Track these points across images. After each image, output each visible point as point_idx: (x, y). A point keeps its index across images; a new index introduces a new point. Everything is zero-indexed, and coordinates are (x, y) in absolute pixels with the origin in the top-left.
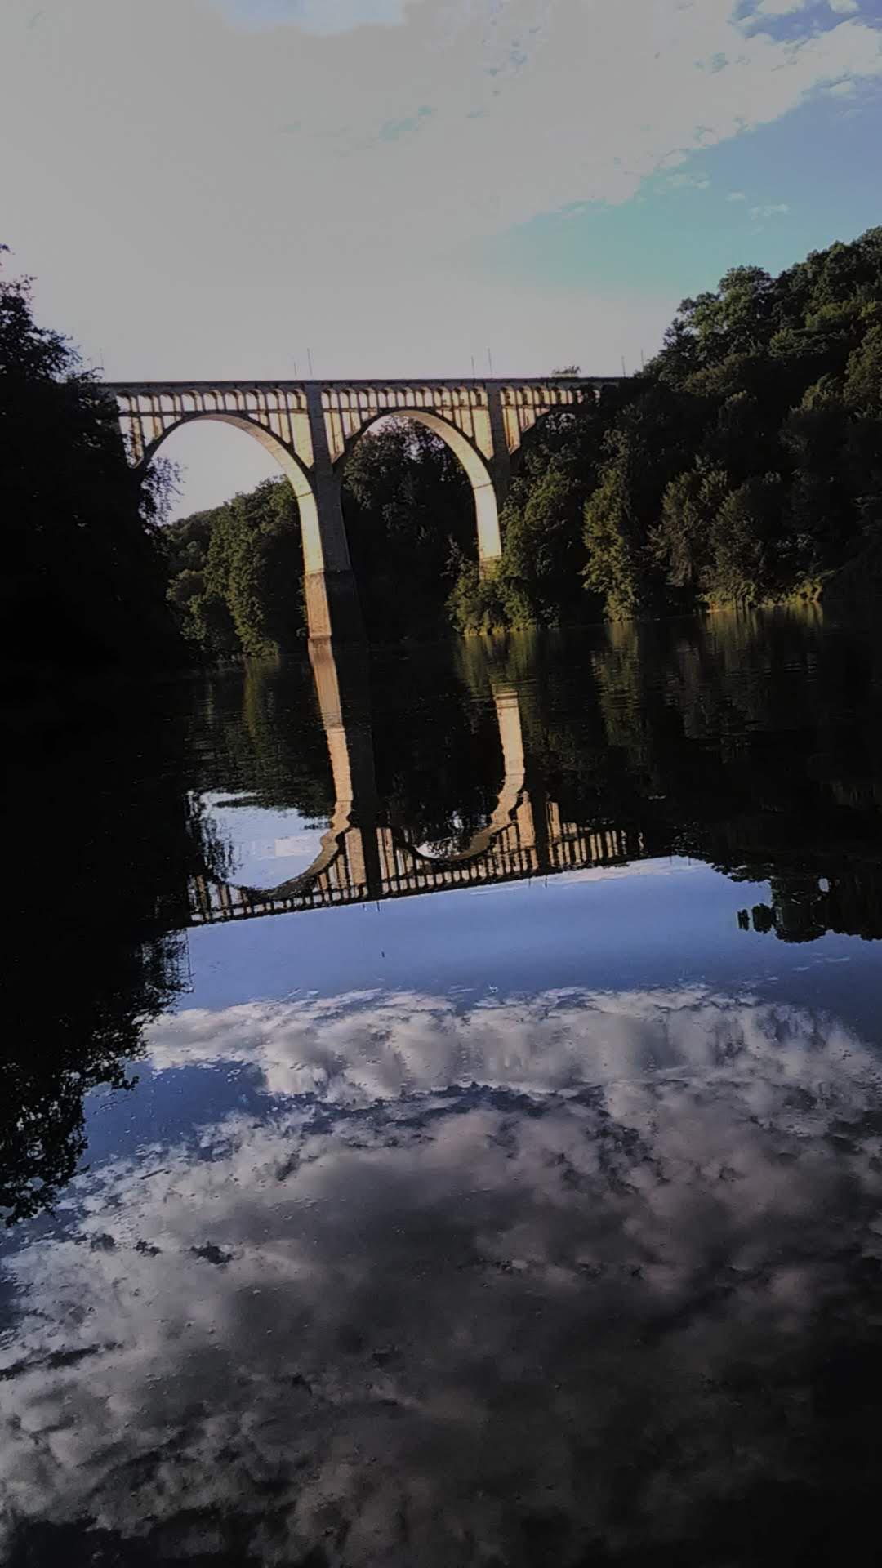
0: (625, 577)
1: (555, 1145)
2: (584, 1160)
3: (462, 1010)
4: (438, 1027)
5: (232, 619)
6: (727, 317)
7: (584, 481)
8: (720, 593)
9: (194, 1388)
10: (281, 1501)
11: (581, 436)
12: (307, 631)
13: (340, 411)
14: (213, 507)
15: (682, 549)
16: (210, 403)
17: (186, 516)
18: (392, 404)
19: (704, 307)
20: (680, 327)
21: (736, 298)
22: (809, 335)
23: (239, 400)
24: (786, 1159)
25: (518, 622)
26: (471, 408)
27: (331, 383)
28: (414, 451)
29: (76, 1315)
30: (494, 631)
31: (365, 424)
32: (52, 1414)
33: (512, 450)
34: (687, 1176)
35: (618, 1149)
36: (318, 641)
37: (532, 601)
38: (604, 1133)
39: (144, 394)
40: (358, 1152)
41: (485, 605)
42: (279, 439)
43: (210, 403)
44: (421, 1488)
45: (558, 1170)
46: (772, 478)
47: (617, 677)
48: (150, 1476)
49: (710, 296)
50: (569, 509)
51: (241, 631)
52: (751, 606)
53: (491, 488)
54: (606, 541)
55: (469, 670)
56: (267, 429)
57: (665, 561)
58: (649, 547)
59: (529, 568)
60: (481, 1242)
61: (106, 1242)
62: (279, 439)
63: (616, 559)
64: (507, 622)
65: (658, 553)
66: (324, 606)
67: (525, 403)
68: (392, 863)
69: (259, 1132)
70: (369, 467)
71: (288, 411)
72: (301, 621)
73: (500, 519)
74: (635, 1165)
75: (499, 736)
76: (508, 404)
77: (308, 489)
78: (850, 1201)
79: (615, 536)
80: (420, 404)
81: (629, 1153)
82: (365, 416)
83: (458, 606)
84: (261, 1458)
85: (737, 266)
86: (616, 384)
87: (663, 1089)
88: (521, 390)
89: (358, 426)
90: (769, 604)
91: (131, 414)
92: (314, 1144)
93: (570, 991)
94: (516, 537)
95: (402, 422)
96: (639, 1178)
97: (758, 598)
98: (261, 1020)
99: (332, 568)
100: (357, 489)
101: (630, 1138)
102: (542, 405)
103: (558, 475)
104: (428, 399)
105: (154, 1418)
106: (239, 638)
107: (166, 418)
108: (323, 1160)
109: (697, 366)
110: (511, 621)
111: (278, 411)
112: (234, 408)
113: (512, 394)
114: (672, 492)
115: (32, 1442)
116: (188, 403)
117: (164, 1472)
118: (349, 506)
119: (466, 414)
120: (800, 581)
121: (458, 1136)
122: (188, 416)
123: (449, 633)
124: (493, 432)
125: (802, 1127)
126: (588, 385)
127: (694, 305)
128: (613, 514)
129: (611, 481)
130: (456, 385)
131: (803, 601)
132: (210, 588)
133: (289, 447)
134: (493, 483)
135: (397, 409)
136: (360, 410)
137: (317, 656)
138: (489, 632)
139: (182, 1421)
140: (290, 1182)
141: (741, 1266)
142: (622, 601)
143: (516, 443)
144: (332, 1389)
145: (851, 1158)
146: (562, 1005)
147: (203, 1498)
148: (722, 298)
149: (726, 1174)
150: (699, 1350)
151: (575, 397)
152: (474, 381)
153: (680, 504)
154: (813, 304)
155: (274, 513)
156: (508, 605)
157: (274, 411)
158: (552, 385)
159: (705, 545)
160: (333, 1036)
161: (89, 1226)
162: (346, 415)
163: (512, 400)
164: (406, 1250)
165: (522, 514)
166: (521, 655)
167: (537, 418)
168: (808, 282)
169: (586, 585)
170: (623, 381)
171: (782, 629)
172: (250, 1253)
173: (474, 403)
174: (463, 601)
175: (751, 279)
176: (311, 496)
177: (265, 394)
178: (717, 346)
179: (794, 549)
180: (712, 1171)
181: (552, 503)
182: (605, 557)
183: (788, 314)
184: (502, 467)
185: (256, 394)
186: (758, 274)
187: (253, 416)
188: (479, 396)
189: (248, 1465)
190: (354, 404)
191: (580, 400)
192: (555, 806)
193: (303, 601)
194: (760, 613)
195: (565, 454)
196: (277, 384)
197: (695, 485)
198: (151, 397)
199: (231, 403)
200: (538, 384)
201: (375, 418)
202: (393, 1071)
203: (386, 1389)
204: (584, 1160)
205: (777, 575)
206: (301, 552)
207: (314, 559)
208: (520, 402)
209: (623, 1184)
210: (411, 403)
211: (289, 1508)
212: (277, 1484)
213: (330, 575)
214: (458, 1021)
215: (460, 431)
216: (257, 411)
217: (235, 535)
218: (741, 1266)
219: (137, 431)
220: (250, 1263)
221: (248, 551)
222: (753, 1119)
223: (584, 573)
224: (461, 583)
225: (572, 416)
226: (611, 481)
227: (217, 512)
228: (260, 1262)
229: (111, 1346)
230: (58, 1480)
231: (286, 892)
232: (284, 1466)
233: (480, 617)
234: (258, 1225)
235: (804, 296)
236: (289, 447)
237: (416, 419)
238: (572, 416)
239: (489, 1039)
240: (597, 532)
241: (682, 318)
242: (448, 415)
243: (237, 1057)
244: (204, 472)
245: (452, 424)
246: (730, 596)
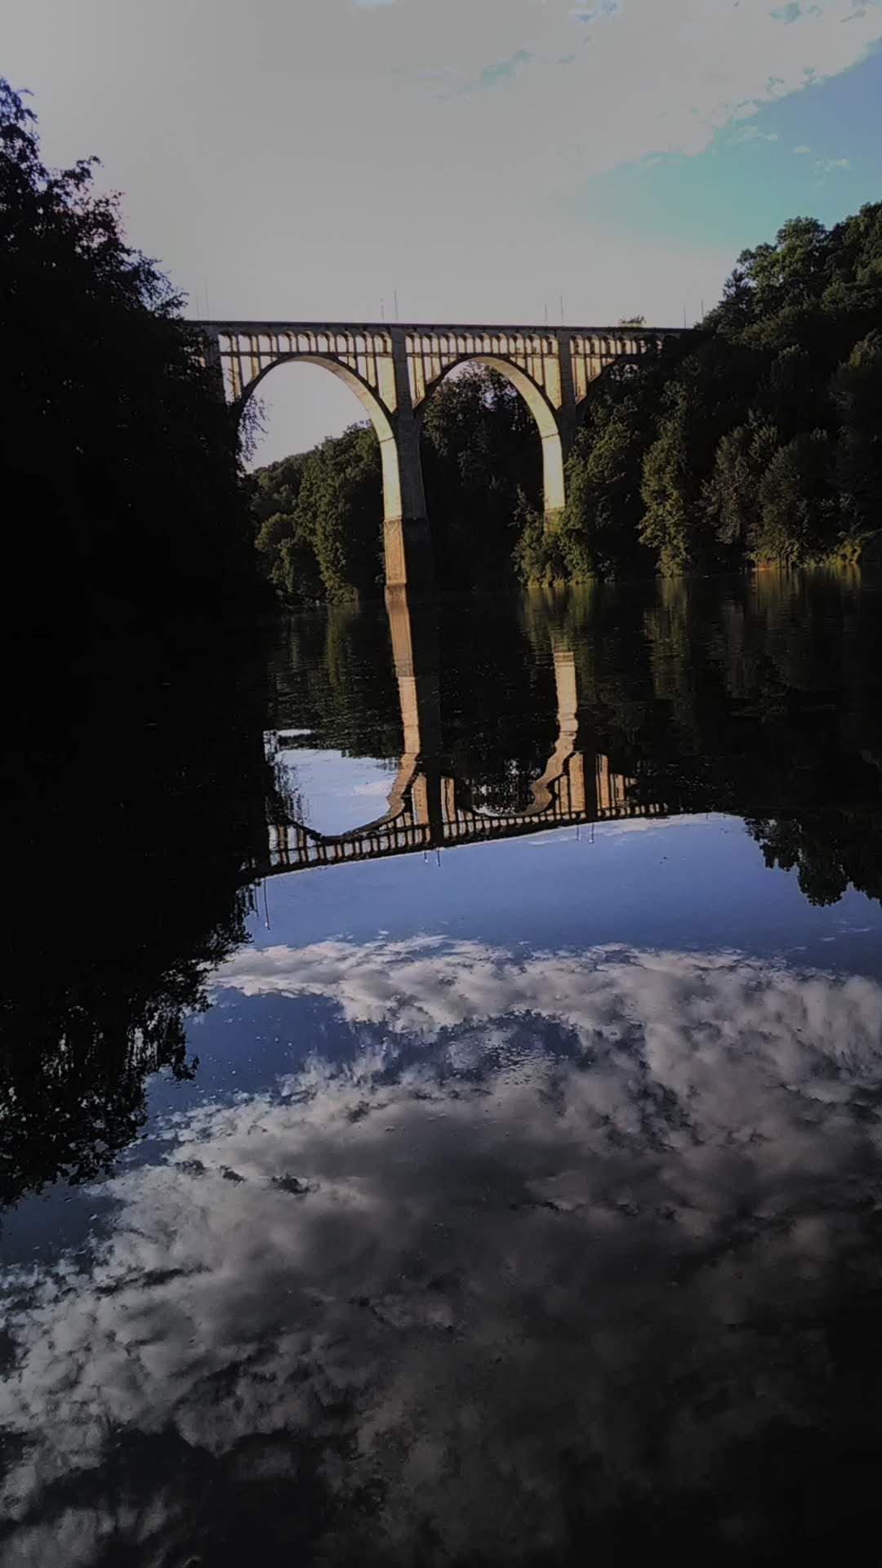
0: (678, 532)
1: (601, 1105)
2: (627, 1121)
3: (519, 960)
4: (498, 975)
5: (318, 563)
6: (783, 269)
7: (643, 433)
8: (766, 552)
9: (272, 1307)
10: (347, 1428)
11: (642, 388)
12: (384, 578)
13: (423, 355)
14: (305, 451)
15: (732, 505)
16: (304, 344)
17: (280, 459)
18: (470, 350)
19: (760, 259)
20: (739, 278)
21: (792, 250)
22: (860, 289)
23: (329, 341)
24: (810, 1126)
25: (577, 576)
26: (542, 356)
27: (415, 327)
28: (489, 398)
29: (165, 1234)
30: (555, 584)
31: (445, 370)
32: (143, 1329)
33: (578, 400)
34: (720, 1138)
35: (658, 1114)
36: (395, 587)
37: (590, 554)
38: (645, 1094)
39: (243, 334)
40: (422, 1102)
41: (548, 557)
42: (365, 382)
43: (304, 344)
44: (469, 1417)
45: (602, 1131)
46: (819, 434)
47: (666, 639)
48: (230, 1393)
49: (767, 247)
50: (629, 463)
51: (326, 575)
52: (794, 565)
53: (557, 438)
54: (661, 495)
56: (355, 372)
57: (716, 517)
58: (701, 503)
59: (589, 521)
60: (531, 1185)
61: (197, 1168)
62: (365, 382)
63: (670, 513)
64: (567, 575)
65: (710, 509)
67: (593, 352)
68: (454, 820)
69: (334, 1084)
70: (446, 414)
71: (375, 355)
72: (379, 568)
73: (565, 470)
74: (673, 1129)
75: (554, 681)
76: (577, 353)
77: (390, 434)
78: (865, 1160)
79: (670, 490)
80: (496, 351)
81: (668, 1118)
82: (445, 361)
83: (523, 558)
84: (328, 1384)
85: (794, 217)
86: (677, 336)
87: (699, 1036)
88: (590, 339)
89: (438, 372)
90: (810, 565)
91: (231, 354)
92: (383, 1093)
93: (615, 947)
94: (579, 489)
95: (481, 371)
96: (676, 1140)
97: (801, 558)
98: (338, 960)
99: (409, 515)
101: (667, 1102)
103: (620, 426)
104: (503, 346)
105: (237, 1336)
107: (263, 358)
108: (387, 1108)
109: (751, 318)
110: (570, 574)
111: (365, 354)
113: (580, 342)
114: (725, 446)
115: (125, 1354)
116: (284, 344)
117: (242, 1388)
118: (427, 450)
119: (537, 361)
120: (841, 541)
121: (513, 1088)
122: (283, 357)
123: (513, 583)
125: (823, 1093)
126: (651, 335)
127: (753, 256)
128: (669, 469)
129: (669, 434)
130: (529, 332)
131: (843, 563)
132: (299, 531)
133: (374, 391)
134: (560, 433)
135: (475, 355)
136: (441, 355)
137: (392, 603)
138: (551, 584)
139: (260, 1338)
140: (362, 1125)
141: (765, 1213)
142: (673, 557)
143: (583, 393)
144: (397, 1315)
145: (868, 1126)
146: (610, 958)
147: (276, 1419)
148: (779, 250)
149: (756, 1138)
150: (725, 1293)
151: (639, 348)
152: (546, 329)
153: (732, 460)
154: (865, 257)
155: (360, 458)
156: (569, 557)
157: (362, 354)
158: (618, 334)
159: (753, 501)
160: (404, 977)
161: (182, 1154)
162: (427, 359)
163: (581, 349)
164: (464, 1187)
165: (585, 466)
166: (579, 610)
167: (603, 368)
168: (861, 235)
169: (641, 540)
170: (684, 332)
171: (820, 590)
172: (326, 1187)
173: (545, 351)
174: (528, 552)
175: (807, 231)
178: (773, 298)
179: (836, 509)
180: (743, 1135)
181: (614, 457)
182: (661, 514)
183: (839, 266)
184: (570, 417)
185: (346, 337)
186: (813, 226)
187: (342, 359)
188: (550, 344)
189: (318, 1387)
190: (435, 350)
191: (643, 350)
192: (604, 758)
193: (381, 548)
194: (802, 573)
195: (627, 405)
196: (366, 327)
197: (748, 439)
198: (250, 336)
199: (323, 345)
200: (605, 333)
201: (455, 364)
202: (458, 1003)
203: (439, 1315)
204: (627, 1121)
205: (819, 536)
206: (382, 496)
207: (393, 508)
209: (662, 1144)
210: (487, 350)
211: (353, 1434)
212: (343, 1408)
213: (407, 523)
214: (515, 970)
215: (532, 379)
217: (323, 480)
218: (765, 1213)
219: (236, 369)
220: (326, 1194)
221: (334, 495)
222: (783, 1086)
224: (527, 532)
225: (635, 367)
226: (669, 434)
227: (306, 457)
228: (334, 1197)
229: (200, 1268)
230: (148, 1388)
232: (350, 1391)
234: (331, 1159)
235: (856, 248)
236: (374, 391)
237: (491, 365)
238: (635, 367)
239: (544, 984)
240: (654, 485)
241: (742, 269)
242: (521, 362)
243: (316, 989)
244: (294, 417)
245: (524, 371)
246: (774, 554)
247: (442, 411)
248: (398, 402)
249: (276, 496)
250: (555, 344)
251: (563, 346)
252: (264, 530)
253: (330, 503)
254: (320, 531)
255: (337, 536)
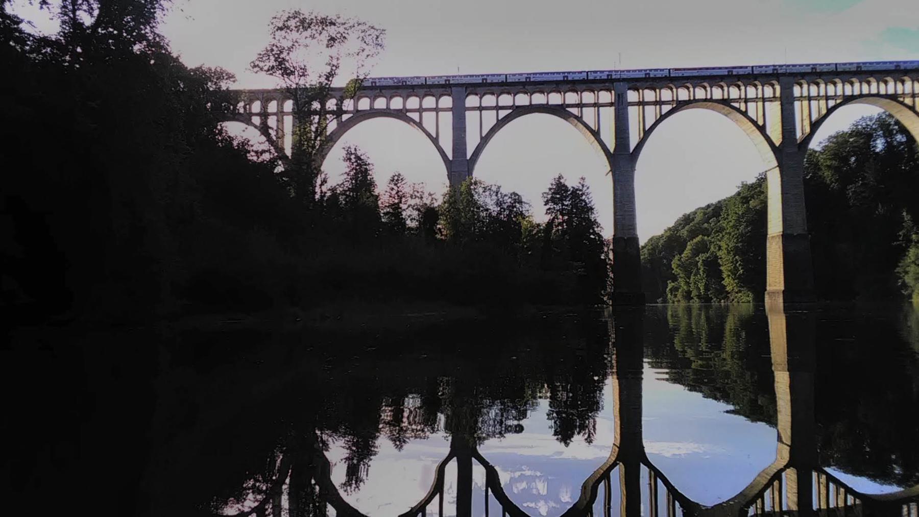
13: (810, 98)
14: (729, 196)
16: (539, 99)
28: (879, 145)
36: (773, 293)
42: (755, 123)
43: (539, 99)
56: (745, 114)
62: (755, 123)
71: (764, 100)
80: (883, 92)
83: (907, 273)
89: (824, 111)
106: (724, 287)
111: (755, 100)
112: (720, 97)
132: (712, 249)
133: (762, 129)
136: (827, 98)
137: (771, 310)
174: (912, 269)
176: (777, 170)
177: (677, 88)
187: (736, 105)
190: (822, 93)
199: (555, 99)
207: (775, 225)
247: (835, 154)
248: (783, 137)
249: (706, 225)
252: (689, 247)
253: (734, 226)
255: (736, 251)
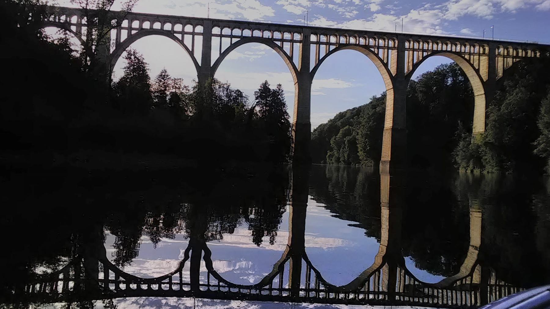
5: (357, 148)
25: (488, 168)
28: (450, 81)
30: (475, 171)
41: (472, 156)
53: (484, 96)
55: (458, 186)
62: (382, 61)
64: (482, 167)
66: (389, 146)
73: (486, 113)
80: (454, 50)
83: (458, 155)
94: (495, 121)
100: (420, 95)
102: (517, 56)
110: (484, 167)
112: (364, 44)
119: (476, 57)
123: (450, 170)
124: (489, 67)
130: (472, 42)
137: (382, 170)
138: (472, 171)
143: (501, 74)
169: (535, 151)
174: (460, 153)
199: (267, 34)
200: (516, 45)
207: (388, 123)
208: (506, 54)
210: (449, 49)
215: (472, 65)
216: (374, 47)
223: (535, 143)
224: (461, 143)
231: (346, 290)
233: (468, 163)
242: (467, 57)
245: (468, 61)
250: (487, 49)
251: (492, 51)
253: (366, 122)
254: (360, 133)
